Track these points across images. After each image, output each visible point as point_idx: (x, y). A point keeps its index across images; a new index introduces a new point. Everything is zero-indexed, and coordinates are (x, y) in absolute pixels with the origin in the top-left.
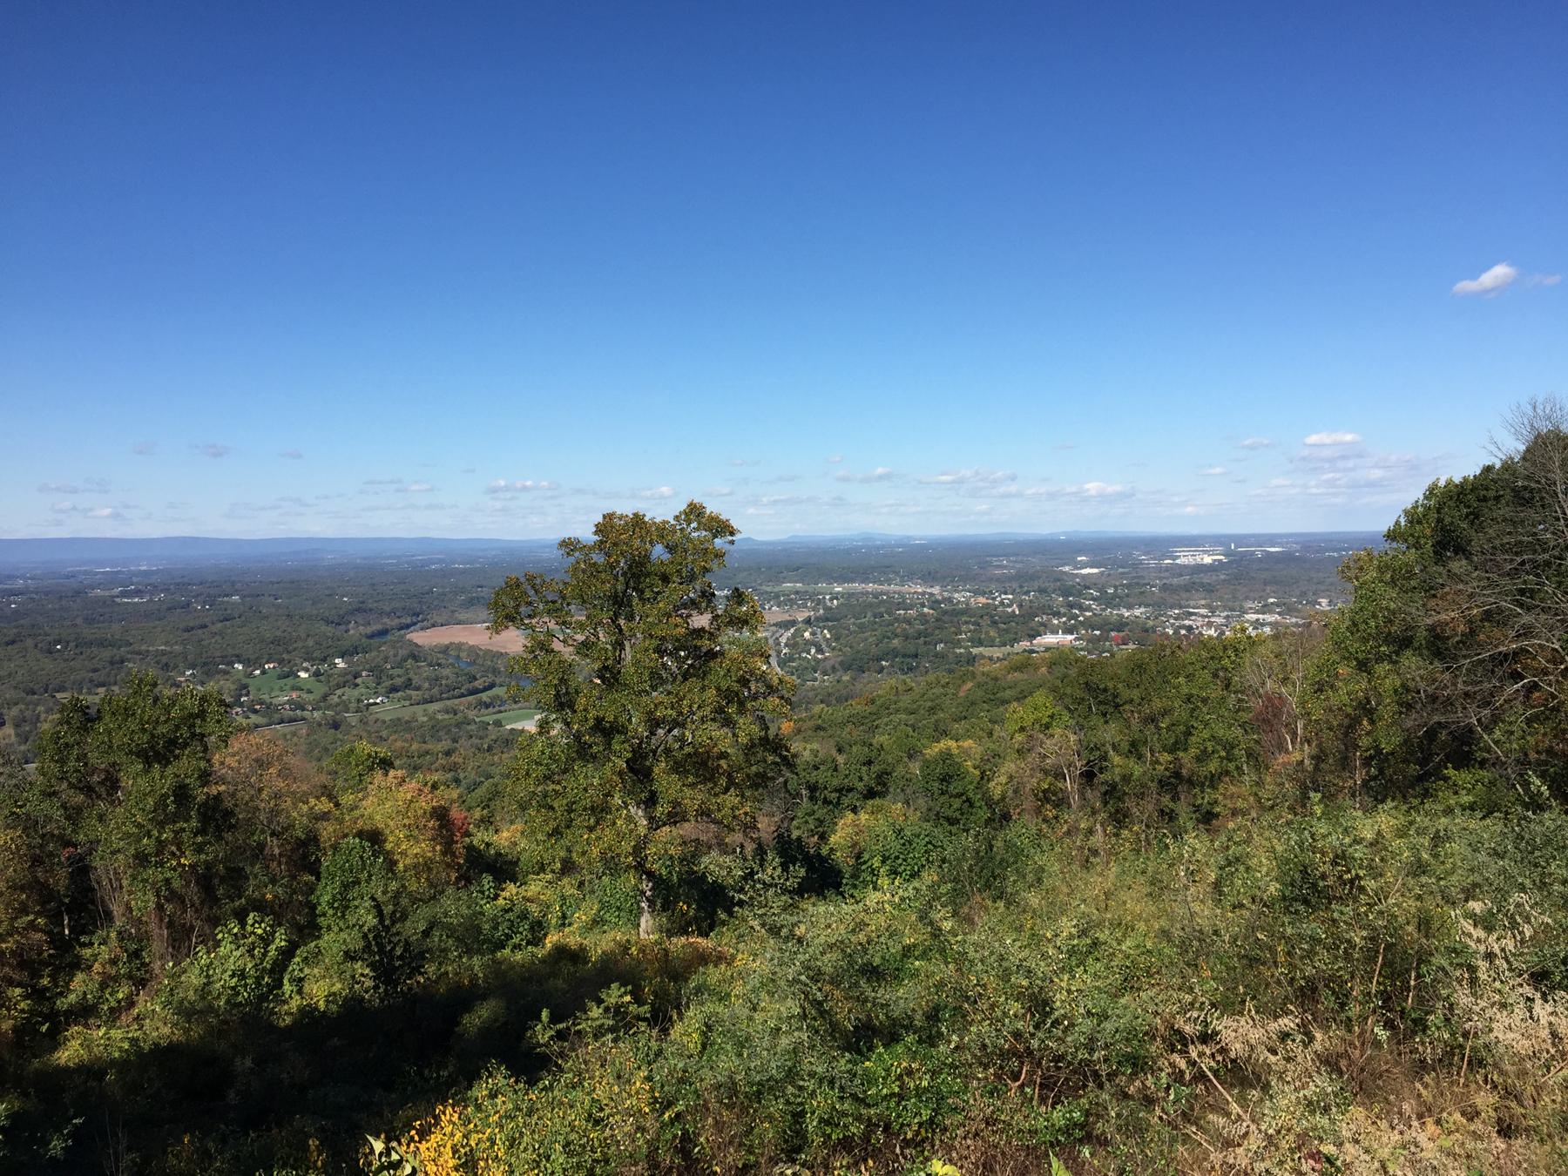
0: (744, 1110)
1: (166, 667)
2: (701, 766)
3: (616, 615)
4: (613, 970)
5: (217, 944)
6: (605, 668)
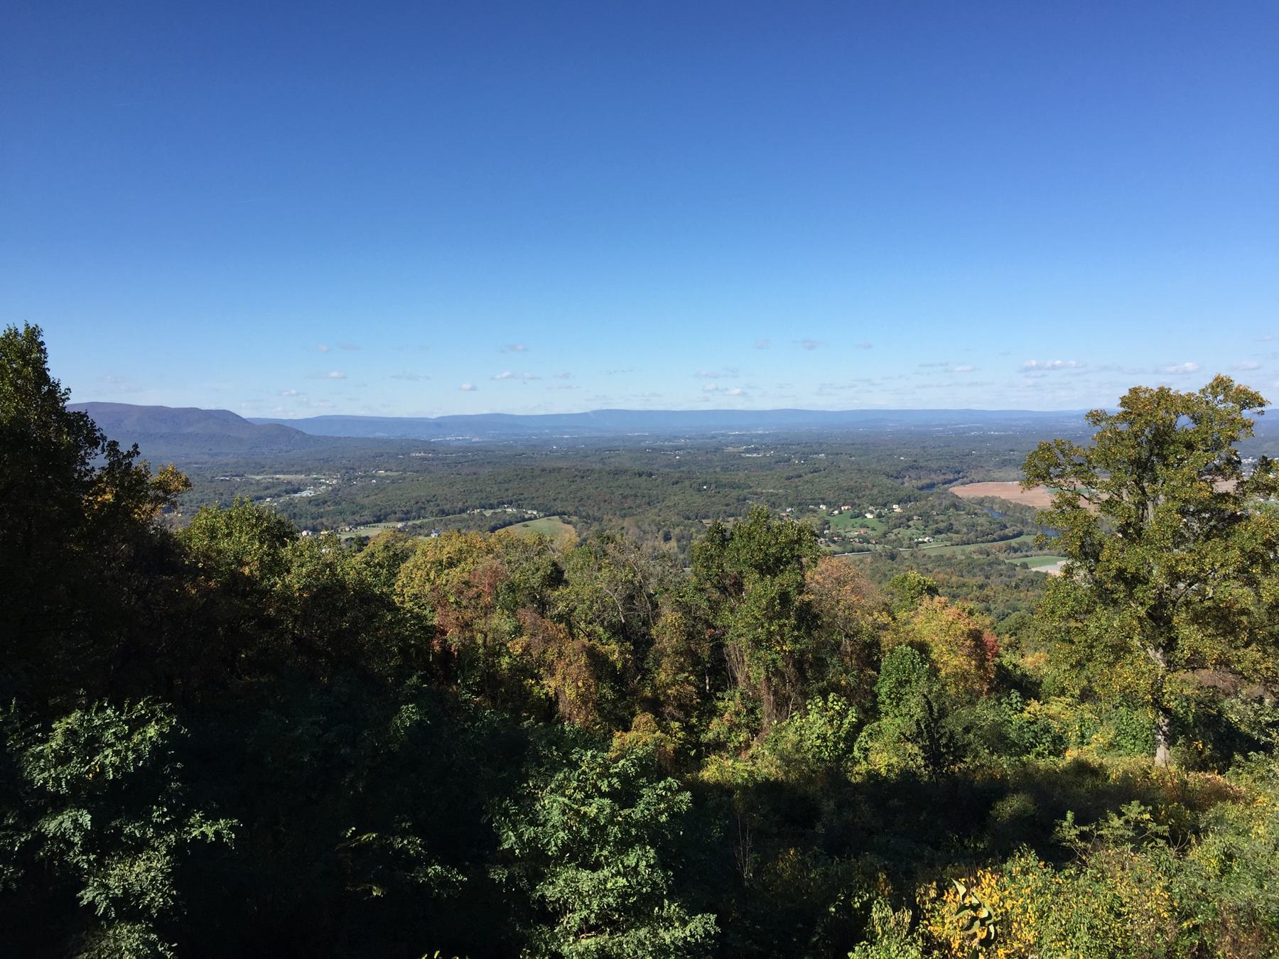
0: (1263, 937)
1: (773, 505)
2: (1222, 620)
3: (1141, 478)
4: (1126, 791)
5: (807, 713)
6: (1128, 525)
